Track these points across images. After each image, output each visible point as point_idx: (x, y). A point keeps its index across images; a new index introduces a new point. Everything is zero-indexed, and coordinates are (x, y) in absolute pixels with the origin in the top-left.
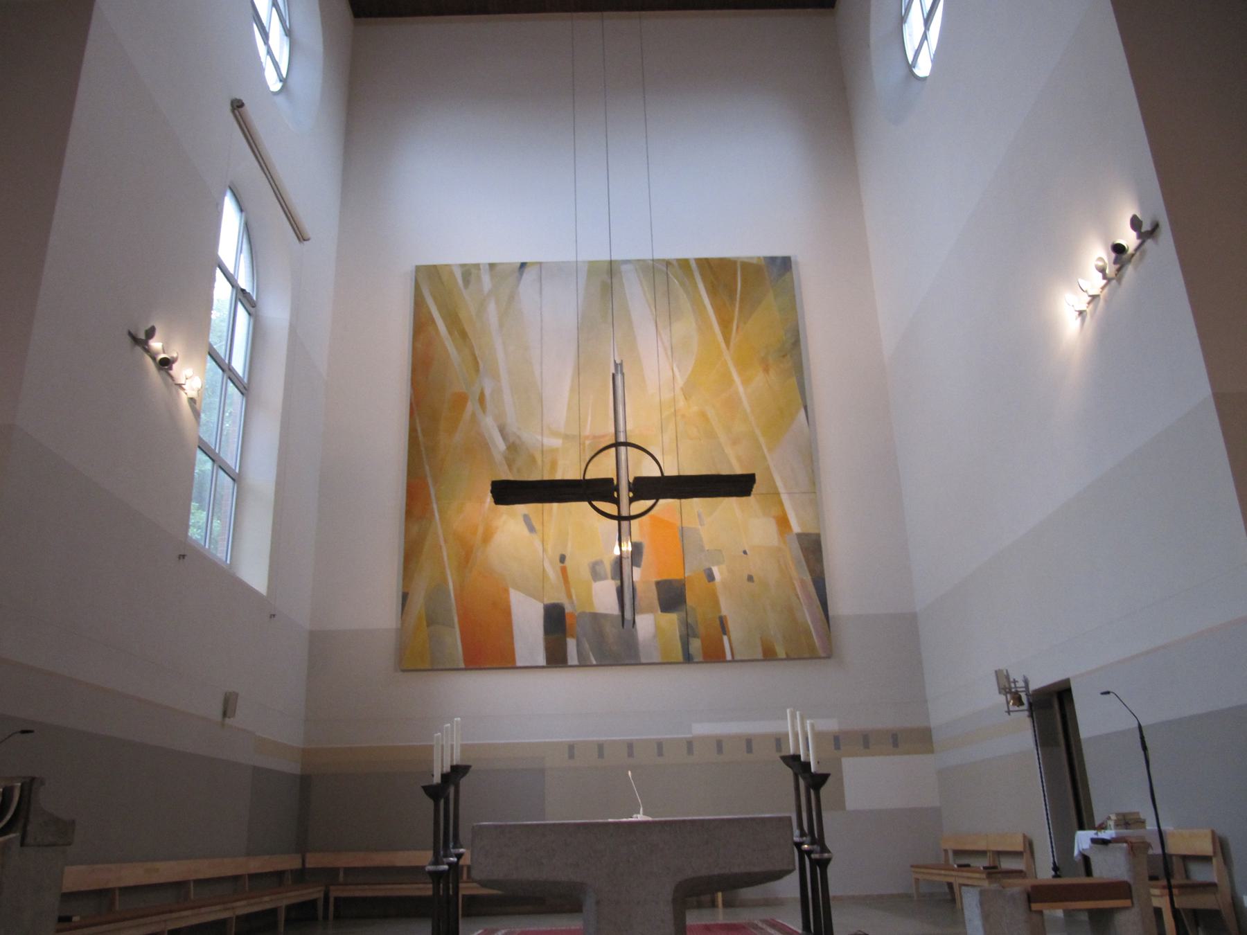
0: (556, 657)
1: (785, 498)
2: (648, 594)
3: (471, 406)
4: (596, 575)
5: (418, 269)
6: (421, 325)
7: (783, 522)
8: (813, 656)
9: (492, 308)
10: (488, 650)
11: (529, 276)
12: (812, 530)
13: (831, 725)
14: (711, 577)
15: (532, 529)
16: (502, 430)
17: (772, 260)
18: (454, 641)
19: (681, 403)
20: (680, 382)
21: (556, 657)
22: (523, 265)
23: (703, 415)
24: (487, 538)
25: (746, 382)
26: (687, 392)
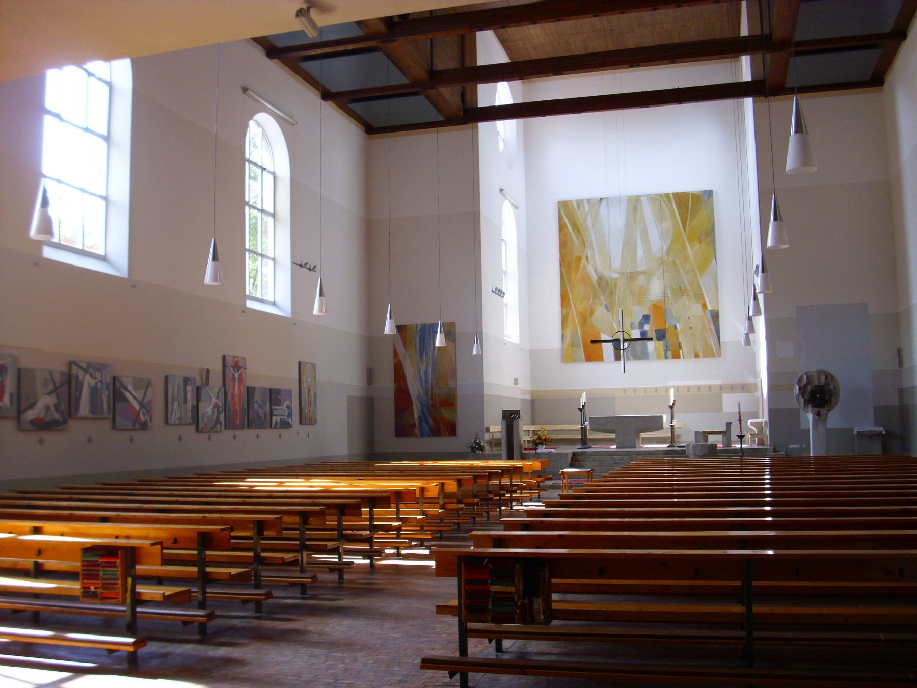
1: (705, 296)
3: (583, 261)
4: (632, 328)
5: (559, 203)
7: (704, 306)
8: (713, 356)
9: (589, 219)
11: (604, 203)
12: (715, 309)
13: (719, 382)
14: (676, 328)
15: (608, 310)
16: (595, 271)
17: (705, 191)
19: (666, 258)
20: (665, 249)
22: (601, 199)
23: (674, 263)
24: (592, 313)
25: (692, 247)
26: (668, 253)
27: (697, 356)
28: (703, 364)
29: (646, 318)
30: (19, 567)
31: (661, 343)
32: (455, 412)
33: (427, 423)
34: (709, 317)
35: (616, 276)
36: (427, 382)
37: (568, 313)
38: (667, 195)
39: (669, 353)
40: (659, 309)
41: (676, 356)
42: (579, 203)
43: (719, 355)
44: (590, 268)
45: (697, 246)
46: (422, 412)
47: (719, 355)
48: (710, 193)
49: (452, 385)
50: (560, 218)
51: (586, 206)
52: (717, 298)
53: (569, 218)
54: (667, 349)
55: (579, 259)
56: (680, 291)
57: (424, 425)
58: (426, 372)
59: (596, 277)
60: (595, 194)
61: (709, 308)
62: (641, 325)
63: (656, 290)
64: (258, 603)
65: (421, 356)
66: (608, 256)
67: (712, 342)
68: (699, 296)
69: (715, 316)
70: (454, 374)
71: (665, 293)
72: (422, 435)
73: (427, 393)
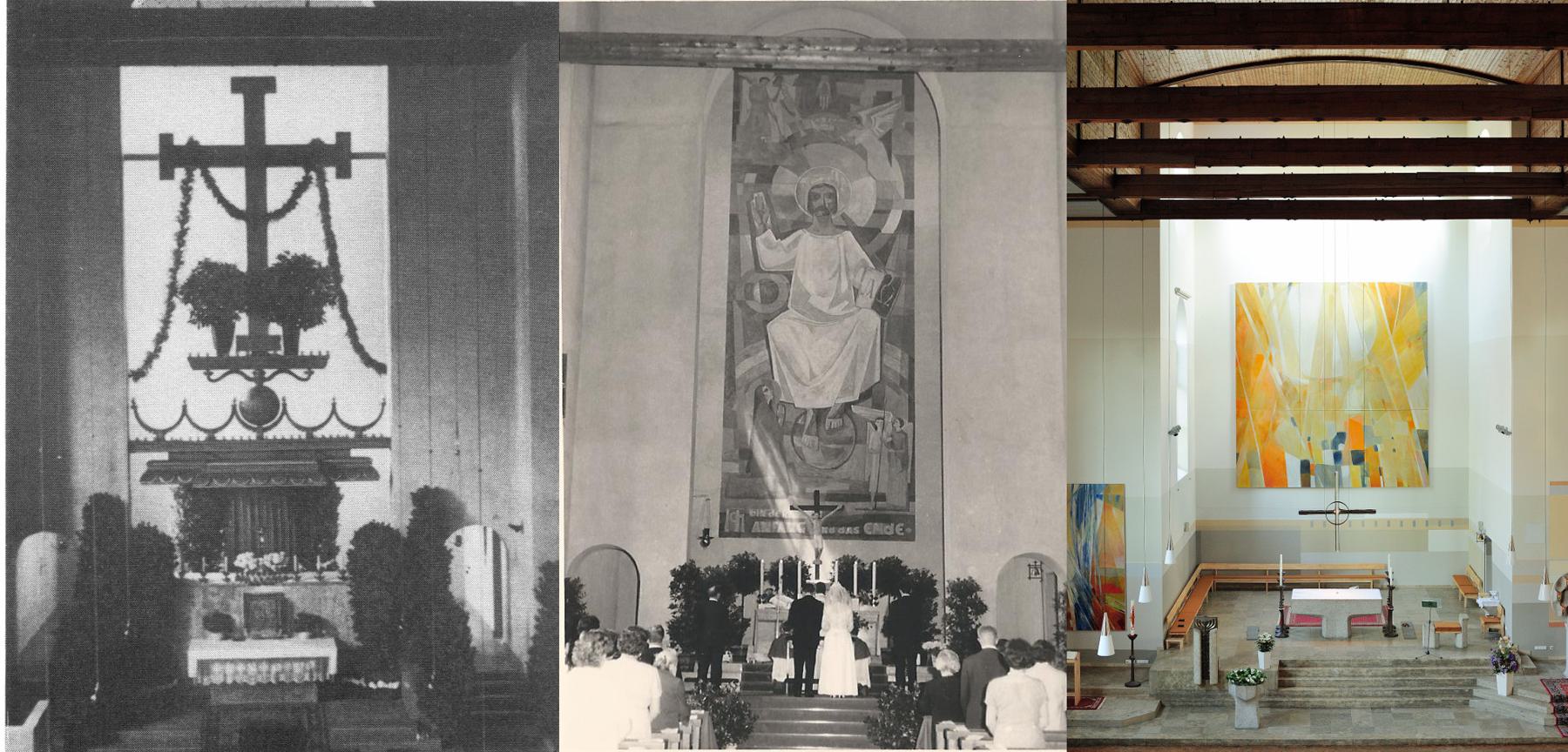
0: (1306, 484)
2: (1347, 457)
3: (1266, 361)
4: (1325, 448)
6: (1240, 317)
7: (1411, 424)
8: (1419, 485)
10: (1275, 480)
13: (1425, 516)
17: (1418, 284)
18: (1260, 476)
21: (1306, 484)
24: (1274, 428)
26: (1370, 357)
27: (1400, 484)
28: (1406, 494)
29: (1341, 437)
30: (612, 27)
31: (1358, 467)
32: (1124, 599)
33: (1087, 612)
34: (1416, 436)
35: (1306, 382)
36: (1086, 560)
37: (1244, 426)
38: (1372, 286)
39: (1368, 480)
40: (1356, 425)
41: (1375, 484)
42: (1263, 287)
43: (1427, 484)
44: (1274, 371)
45: (1406, 351)
46: (1080, 598)
47: (1427, 484)
48: (1425, 285)
49: (1119, 565)
50: (1238, 305)
51: (1271, 291)
52: (1427, 415)
53: (1249, 306)
54: (1364, 474)
55: (1260, 358)
56: (1384, 404)
57: (1083, 616)
58: (1086, 546)
59: (1280, 382)
60: (1283, 279)
61: (1417, 427)
62: (1335, 445)
63: (1354, 402)
64: (760, 48)
65: (1078, 526)
66: (1294, 362)
67: (1419, 468)
68: (1406, 412)
69: (1424, 437)
70: (1123, 553)
71: (1365, 407)
72: (1079, 628)
73: (1086, 575)
